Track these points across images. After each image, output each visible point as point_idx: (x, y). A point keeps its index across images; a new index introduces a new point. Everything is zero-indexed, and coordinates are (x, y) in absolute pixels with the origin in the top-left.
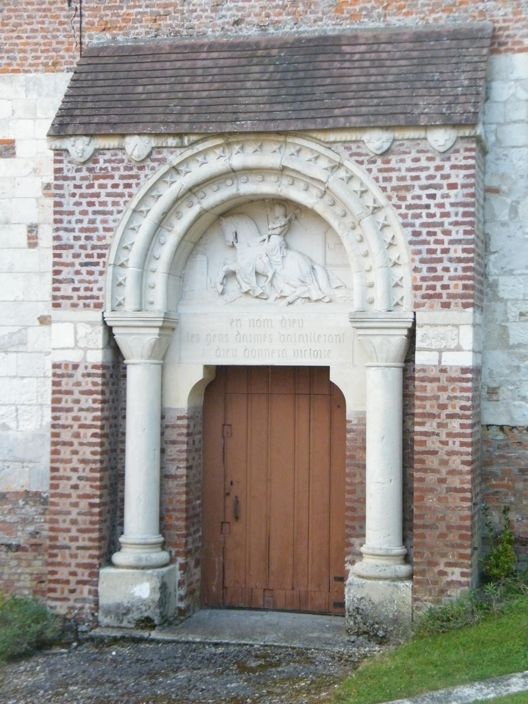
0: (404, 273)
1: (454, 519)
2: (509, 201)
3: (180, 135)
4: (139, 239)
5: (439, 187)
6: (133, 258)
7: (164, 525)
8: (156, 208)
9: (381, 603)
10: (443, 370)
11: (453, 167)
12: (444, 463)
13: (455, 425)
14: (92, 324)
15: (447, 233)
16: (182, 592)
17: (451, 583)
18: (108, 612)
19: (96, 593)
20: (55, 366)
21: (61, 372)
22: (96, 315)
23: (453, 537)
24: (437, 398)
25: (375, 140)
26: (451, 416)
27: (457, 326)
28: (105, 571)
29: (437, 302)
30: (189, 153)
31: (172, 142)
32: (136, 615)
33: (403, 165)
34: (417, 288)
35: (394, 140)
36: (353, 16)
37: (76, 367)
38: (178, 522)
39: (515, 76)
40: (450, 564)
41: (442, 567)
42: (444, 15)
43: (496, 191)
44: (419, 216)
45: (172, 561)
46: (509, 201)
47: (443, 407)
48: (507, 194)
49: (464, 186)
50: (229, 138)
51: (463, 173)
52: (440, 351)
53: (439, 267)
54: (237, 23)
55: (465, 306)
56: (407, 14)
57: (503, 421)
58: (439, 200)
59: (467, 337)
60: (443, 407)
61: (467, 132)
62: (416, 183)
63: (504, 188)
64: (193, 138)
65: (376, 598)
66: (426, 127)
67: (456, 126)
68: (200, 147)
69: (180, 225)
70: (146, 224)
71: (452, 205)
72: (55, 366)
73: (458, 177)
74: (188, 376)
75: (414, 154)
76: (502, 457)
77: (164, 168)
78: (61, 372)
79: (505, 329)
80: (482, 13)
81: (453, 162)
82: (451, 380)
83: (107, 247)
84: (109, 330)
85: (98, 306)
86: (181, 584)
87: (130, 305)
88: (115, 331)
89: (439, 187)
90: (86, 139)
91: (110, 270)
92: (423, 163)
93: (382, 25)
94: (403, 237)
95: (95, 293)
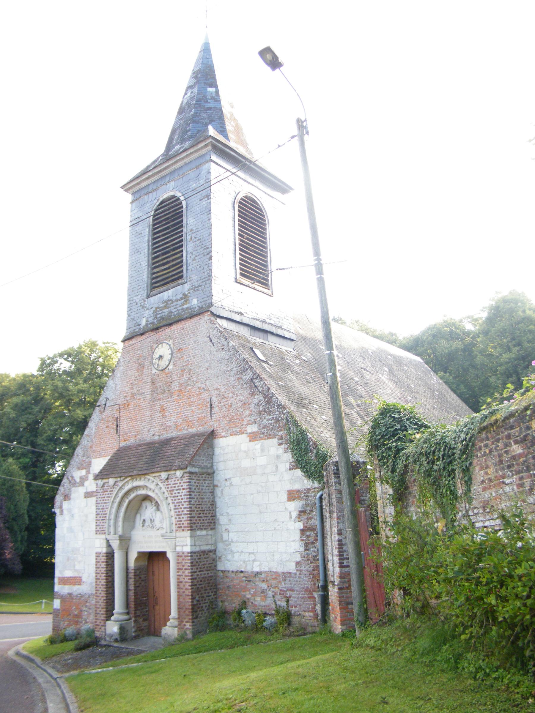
0: (174, 520)
1: (187, 606)
2: (220, 489)
3: (120, 477)
4: (114, 511)
5: (180, 489)
6: (112, 517)
7: (127, 606)
8: (118, 500)
9: (170, 635)
10: (183, 553)
11: (184, 482)
12: (184, 586)
13: (186, 572)
14: (103, 539)
15: (183, 505)
16: (133, 630)
17: (187, 628)
18: (108, 636)
19: (105, 629)
20: (96, 553)
21: (98, 555)
22: (104, 536)
23: (187, 612)
24: (182, 563)
25: (164, 475)
26: (186, 569)
27: (186, 537)
28: (108, 622)
29: (181, 529)
30: (124, 482)
31: (119, 479)
32: (114, 637)
33: (171, 482)
34: (176, 524)
35: (169, 475)
36: (180, 430)
37: (100, 553)
38: (132, 605)
39: (220, 446)
40: (187, 622)
41: (184, 623)
42: (202, 427)
43: (217, 486)
44: (175, 500)
45: (130, 619)
46: (220, 489)
47: (183, 566)
48: (220, 487)
49: (187, 489)
50: (133, 477)
51: (186, 484)
52: (182, 546)
53: (181, 517)
54: (153, 435)
55: (188, 530)
56: (193, 428)
57: (223, 569)
58: (180, 494)
59: (188, 541)
60: (183, 566)
61: (185, 471)
62: (175, 489)
63: (219, 485)
64: (123, 478)
65: (169, 633)
66: (175, 470)
67: (182, 469)
68: (126, 480)
69: (125, 505)
70: (116, 505)
71: (184, 495)
72: (96, 553)
73: (185, 486)
74: (133, 556)
75: (174, 479)
76: (222, 582)
77: (118, 488)
78: (98, 555)
79: (222, 535)
80: (211, 426)
81: (184, 481)
82: (185, 556)
83: (106, 514)
84: (108, 541)
85: (105, 533)
86: (134, 627)
87: (112, 532)
88: (110, 541)
89: (180, 489)
90: (100, 480)
91: (107, 521)
92: (177, 482)
93: (187, 432)
94: (172, 506)
95: (104, 529)
